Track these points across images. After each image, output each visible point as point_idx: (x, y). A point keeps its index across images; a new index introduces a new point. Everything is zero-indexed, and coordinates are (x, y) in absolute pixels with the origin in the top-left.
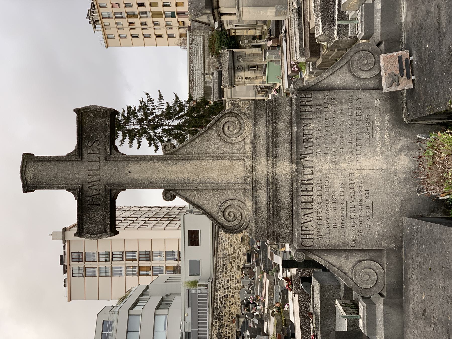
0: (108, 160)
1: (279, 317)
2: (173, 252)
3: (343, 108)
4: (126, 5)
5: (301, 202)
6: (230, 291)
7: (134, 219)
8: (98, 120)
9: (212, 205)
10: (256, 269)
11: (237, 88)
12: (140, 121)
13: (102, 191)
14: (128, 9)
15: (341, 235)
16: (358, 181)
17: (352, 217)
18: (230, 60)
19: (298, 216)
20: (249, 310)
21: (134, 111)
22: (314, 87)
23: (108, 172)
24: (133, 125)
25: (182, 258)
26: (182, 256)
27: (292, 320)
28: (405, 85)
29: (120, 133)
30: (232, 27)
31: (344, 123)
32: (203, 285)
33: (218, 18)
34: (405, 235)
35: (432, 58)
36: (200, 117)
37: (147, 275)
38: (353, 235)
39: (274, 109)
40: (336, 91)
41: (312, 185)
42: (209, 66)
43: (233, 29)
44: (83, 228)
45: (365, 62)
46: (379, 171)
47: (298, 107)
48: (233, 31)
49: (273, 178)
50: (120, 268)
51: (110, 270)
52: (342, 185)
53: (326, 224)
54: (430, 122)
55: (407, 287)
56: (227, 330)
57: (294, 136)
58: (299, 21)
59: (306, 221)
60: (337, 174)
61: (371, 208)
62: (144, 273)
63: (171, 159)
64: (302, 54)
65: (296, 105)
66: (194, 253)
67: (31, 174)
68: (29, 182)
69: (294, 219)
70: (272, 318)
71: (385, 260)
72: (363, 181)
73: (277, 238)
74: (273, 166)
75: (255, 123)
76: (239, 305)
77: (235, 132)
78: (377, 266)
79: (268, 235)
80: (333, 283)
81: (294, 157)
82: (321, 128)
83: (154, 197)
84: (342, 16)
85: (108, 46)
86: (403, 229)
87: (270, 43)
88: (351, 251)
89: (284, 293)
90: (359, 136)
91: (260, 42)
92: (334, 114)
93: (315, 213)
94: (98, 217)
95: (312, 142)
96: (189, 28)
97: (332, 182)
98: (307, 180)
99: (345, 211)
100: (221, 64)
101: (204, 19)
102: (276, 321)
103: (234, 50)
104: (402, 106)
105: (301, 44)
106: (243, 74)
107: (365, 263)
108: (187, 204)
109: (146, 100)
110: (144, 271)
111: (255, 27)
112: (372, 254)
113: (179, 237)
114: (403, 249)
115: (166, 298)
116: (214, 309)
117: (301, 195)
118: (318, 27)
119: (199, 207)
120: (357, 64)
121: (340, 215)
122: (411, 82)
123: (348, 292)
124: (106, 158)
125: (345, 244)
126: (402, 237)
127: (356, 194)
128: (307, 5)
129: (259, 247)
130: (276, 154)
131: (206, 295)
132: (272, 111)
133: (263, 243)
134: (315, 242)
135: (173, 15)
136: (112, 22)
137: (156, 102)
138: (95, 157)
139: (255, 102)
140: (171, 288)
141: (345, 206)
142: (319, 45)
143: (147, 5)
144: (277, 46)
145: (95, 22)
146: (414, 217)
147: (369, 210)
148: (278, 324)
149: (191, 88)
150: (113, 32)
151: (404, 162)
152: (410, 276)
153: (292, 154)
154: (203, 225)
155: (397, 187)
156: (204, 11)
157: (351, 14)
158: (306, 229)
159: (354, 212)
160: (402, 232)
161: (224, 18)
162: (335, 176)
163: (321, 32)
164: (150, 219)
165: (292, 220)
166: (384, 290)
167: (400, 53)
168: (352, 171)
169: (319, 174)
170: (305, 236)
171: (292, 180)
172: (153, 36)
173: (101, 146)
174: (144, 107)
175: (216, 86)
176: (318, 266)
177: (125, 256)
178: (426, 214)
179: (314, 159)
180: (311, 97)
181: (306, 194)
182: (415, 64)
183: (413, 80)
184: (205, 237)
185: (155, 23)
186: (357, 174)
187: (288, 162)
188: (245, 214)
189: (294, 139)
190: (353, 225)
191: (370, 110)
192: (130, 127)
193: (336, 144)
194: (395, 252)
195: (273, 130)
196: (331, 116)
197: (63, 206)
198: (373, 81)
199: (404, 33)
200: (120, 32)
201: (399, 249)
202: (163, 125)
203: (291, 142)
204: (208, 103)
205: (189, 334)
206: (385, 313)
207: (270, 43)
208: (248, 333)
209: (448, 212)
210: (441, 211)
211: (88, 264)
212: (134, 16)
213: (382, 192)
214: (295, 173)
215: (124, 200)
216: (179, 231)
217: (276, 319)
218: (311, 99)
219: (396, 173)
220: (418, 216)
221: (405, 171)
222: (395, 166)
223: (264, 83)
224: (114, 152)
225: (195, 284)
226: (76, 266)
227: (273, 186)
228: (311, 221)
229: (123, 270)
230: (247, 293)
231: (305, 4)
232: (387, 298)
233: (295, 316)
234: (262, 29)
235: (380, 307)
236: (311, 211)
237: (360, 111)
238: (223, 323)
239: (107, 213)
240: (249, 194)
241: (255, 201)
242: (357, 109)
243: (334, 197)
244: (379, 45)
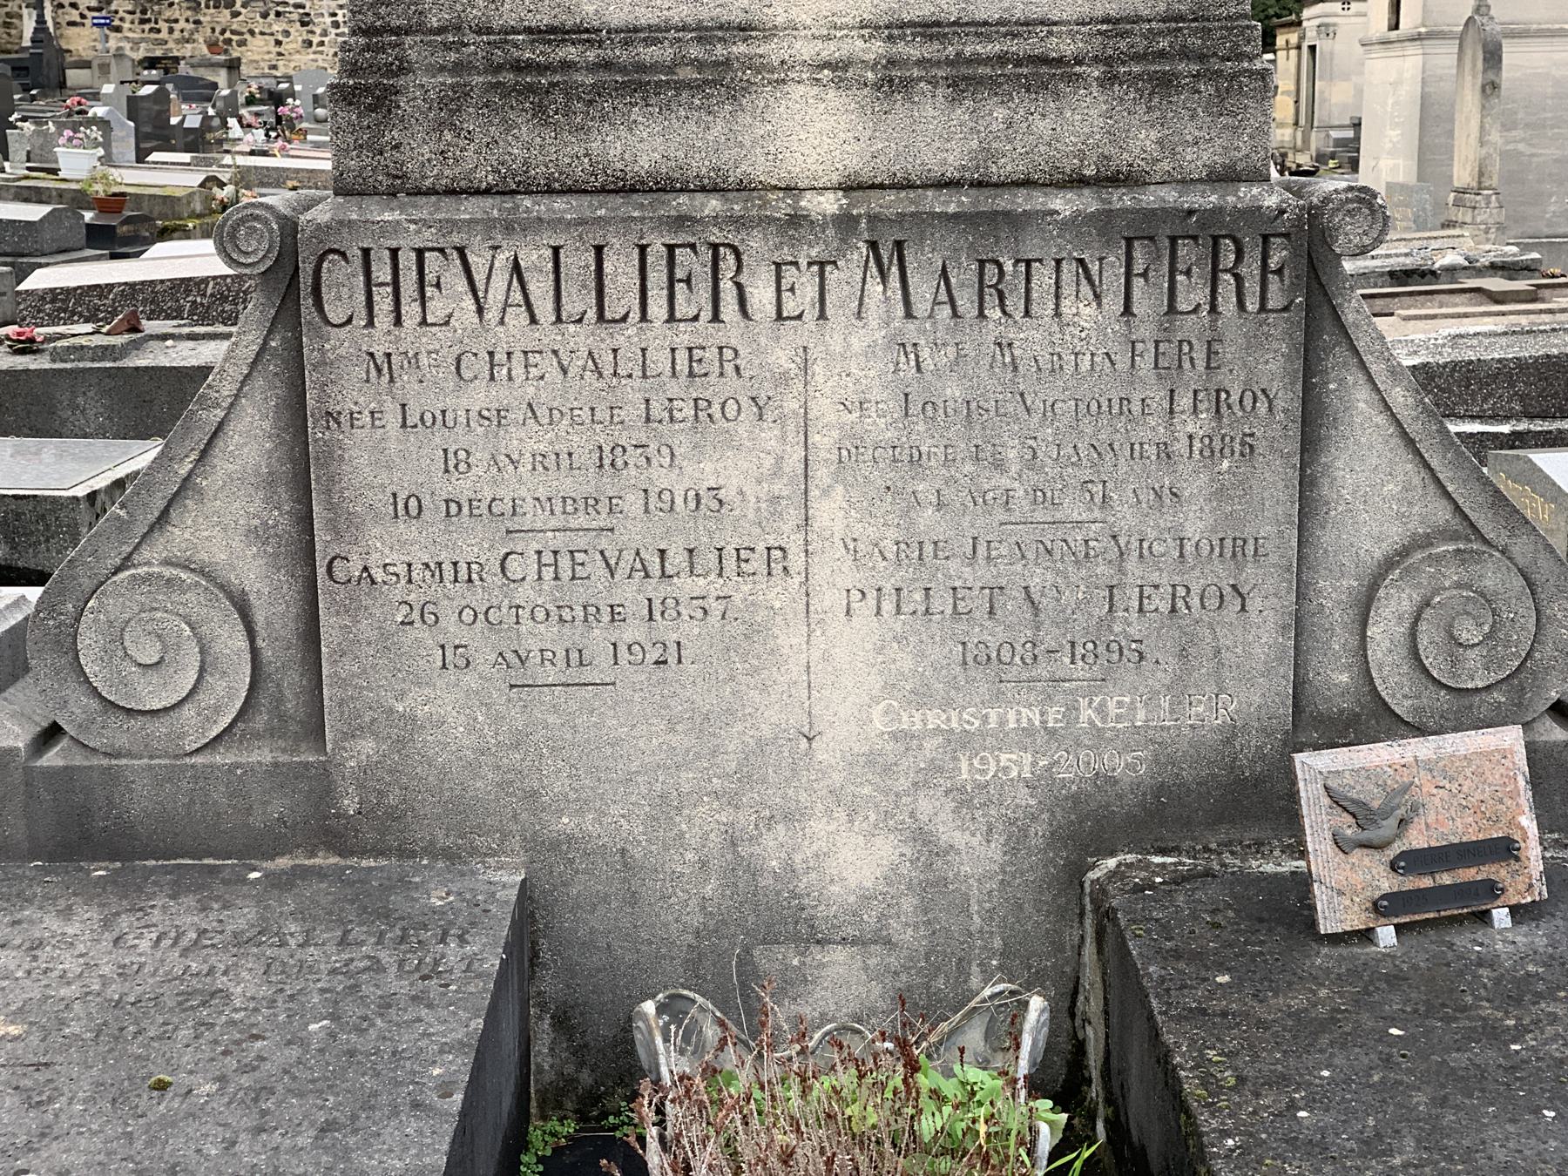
1: (198, 207)
3: (1182, 506)
5: (599, 250)
6: (325, 33)
15: (402, 497)
16: (737, 598)
17: (513, 564)
19: (509, 229)
20: (251, 101)
22: (1328, 324)
27: (159, 249)
28: (1344, 888)
30: (1308, 34)
31: (1097, 514)
34: (417, 870)
38: (401, 569)
39: (1194, 68)
40: (1296, 460)
41: (706, 314)
43: (1302, 38)
45: (1469, 632)
46: (797, 719)
47: (1202, 225)
48: (1294, 38)
49: (749, 63)
53: (465, 402)
54: (1092, 1004)
55: (93, 892)
56: (182, 24)
57: (1022, 201)
58: (1382, 274)
59: (479, 278)
60: (777, 472)
61: (573, 675)
65: (1218, 211)
69: (488, 202)
71: (262, 755)
72: (737, 629)
73: (368, 89)
74: (827, 65)
76: (274, 67)
78: (217, 710)
79: (378, 32)
82: (1069, 369)
86: (450, 855)
88: (302, 555)
90: (1012, 605)
92: (1151, 451)
93: (532, 337)
95: (981, 315)
97: (729, 442)
98: (739, 286)
99: (553, 523)
102: (179, 193)
104: (1186, 844)
107: (230, 642)
111: (1302, 121)
112: (291, 681)
114: (334, 860)
117: (643, 249)
120: (1458, 585)
121: (523, 492)
122: (1354, 920)
126: (404, 853)
128: (1456, 305)
130: (907, 85)
132: (1185, 54)
134: (344, 345)
141: (581, 520)
147: (561, 664)
148: (169, 202)
151: (850, 861)
152: (156, 917)
153: (907, 185)
155: (704, 824)
158: (430, 277)
159: (548, 573)
160: (432, 851)
162: (769, 462)
165: (487, 192)
166: (75, 749)
167: (1533, 854)
168: (796, 561)
169: (782, 358)
170: (382, 273)
171: (743, 187)
178: (549, 983)
179: (873, 331)
180: (1263, 308)
181: (652, 276)
182: (1466, 941)
183: (1366, 935)
186: (779, 594)
187: (854, 164)
190: (463, 568)
191: (1171, 664)
193: (969, 468)
194: (310, 824)
195: (1059, 61)
196: (1142, 434)
198: (1344, 678)
201: (334, 835)
203: (979, 184)
209: (559, 1106)
210: (569, 1069)
213: (674, 740)
214: (781, 207)
217: (191, 195)
218: (1252, 305)
219: (788, 817)
220: (534, 943)
221: (799, 866)
222: (829, 813)
227: (699, 65)
228: (480, 310)
230: (315, 97)
231: (1457, 298)
232: (28, 770)
234: (1296, 150)
236: (545, 309)
237: (1165, 607)
238: (208, 7)
242: (1181, 591)
243: (634, 456)
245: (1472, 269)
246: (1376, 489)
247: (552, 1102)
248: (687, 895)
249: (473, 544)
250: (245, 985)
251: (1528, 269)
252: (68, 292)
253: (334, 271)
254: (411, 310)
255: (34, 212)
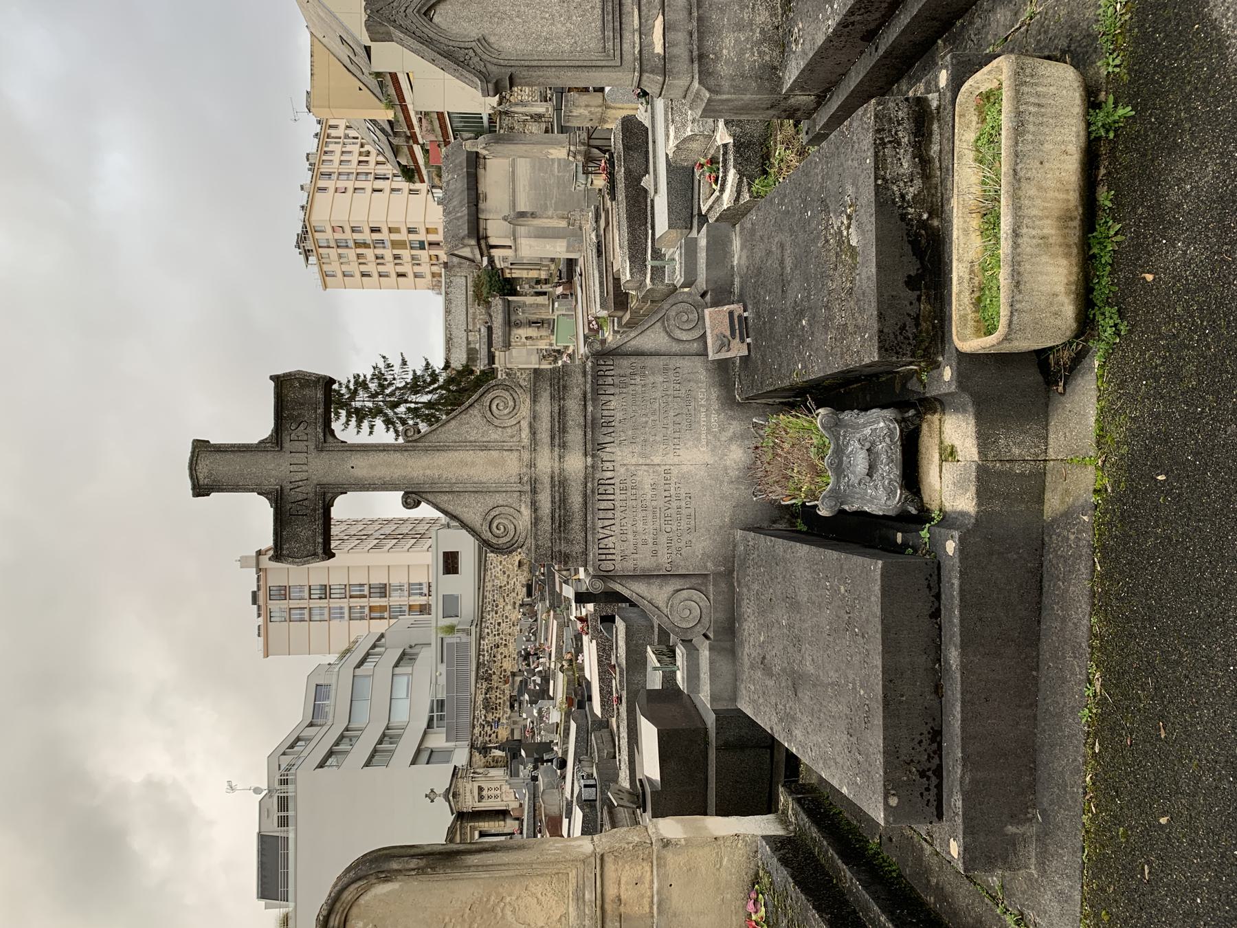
0: (320, 449)
2: (421, 584)
4: (354, 230)
7: (362, 537)
8: (306, 392)
9: (473, 512)
10: (539, 607)
11: (514, 351)
12: (373, 396)
13: (311, 496)
14: (357, 236)
18: (504, 312)
20: (528, 665)
21: (364, 381)
23: (320, 468)
24: (362, 400)
25: (433, 593)
26: (433, 589)
27: (587, 676)
28: (738, 350)
29: (343, 413)
32: (463, 630)
33: (485, 252)
35: (774, 314)
36: (461, 391)
37: (381, 618)
42: (474, 319)
44: (281, 549)
46: (703, 467)
50: (341, 608)
51: (326, 611)
52: (654, 486)
54: (771, 401)
55: (740, 625)
57: (589, 418)
62: (378, 615)
63: (414, 449)
64: (603, 306)
66: (450, 585)
67: (205, 470)
68: (201, 482)
70: (560, 675)
75: (535, 400)
77: (506, 412)
80: (642, 622)
81: (589, 446)
83: (389, 505)
84: (657, 254)
85: (326, 287)
86: (735, 546)
87: (560, 290)
89: (578, 638)
90: (678, 419)
91: (545, 288)
94: (304, 533)
96: (446, 265)
100: (490, 316)
101: (466, 252)
103: (510, 298)
105: (602, 292)
106: (522, 332)
107: (685, 594)
108: (441, 515)
109: (381, 365)
110: (376, 613)
112: (694, 581)
113: (430, 562)
115: (409, 650)
116: (478, 665)
118: (624, 269)
119: (454, 517)
122: (745, 346)
123: (664, 634)
124: (317, 447)
125: (658, 567)
127: (673, 498)
129: (543, 574)
131: (467, 645)
133: (549, 570)
134: (619, 566)
135: (422, 246)
136: (333, 253)
137: (397, 369)
138: (301, 446)
139: (536, 371)
140: (416, 636)
142: (627, 294)
143: (385, 230)
144: (570, 294)
145: (307, 253)
146: (749, 530)
149: (448, 350)
150: (334, 267)
151: (737, 455)
154: (466, 547)
156: (466, 241)
157: (668, 252)
160: (734, 550)
161: (494, 252)
163: (628, 277)
164: (387, 536)
167: (732, 307)
169: (622, 470)
172: (394, 275)
173: (309, 430)
174: (379, 376)
175: (485, 347)
176: (624, 599)
177: (349, 592)
178: (765, 525)
182: (750, 322)
183: (749, 344)
184: (468, 562)
185: (396, 257)
186: (675, 471)
188: (520, 528)
189: (589, 422)
192: (358, 404)
194: (725, 578)
197: (253, 517)
199: (737, 280)
200: (344, 268)
201: (730, 572)
202: (406, 401)
204: (472, 372)
205: (442, 701)
206: (712, 662)
207: (560, 290)
208: (527, 697)
211: (293, 603)
212: (365, 245)
215: (344, 508)
216: (429, 554)
223: (551, 345)
224: (330, 439)
225: (451, 629)
226: (275, 606)
229: (346, 611)
233: (591, 671)
235: (705, 654)
236: (612, 522)
239: (318, 526)
240: (527, 498)
241: (534, 506)
244: (703, 295)
245: (597, 229)
246: (653, 339)
247: (793, 524)
248: (742, 492)
249: (663, 539)
250: (756, 587)
251: (597, 209)
252: (602, 701)
253: (603, 567)
254: (612, 551)
255: (573, 726)
